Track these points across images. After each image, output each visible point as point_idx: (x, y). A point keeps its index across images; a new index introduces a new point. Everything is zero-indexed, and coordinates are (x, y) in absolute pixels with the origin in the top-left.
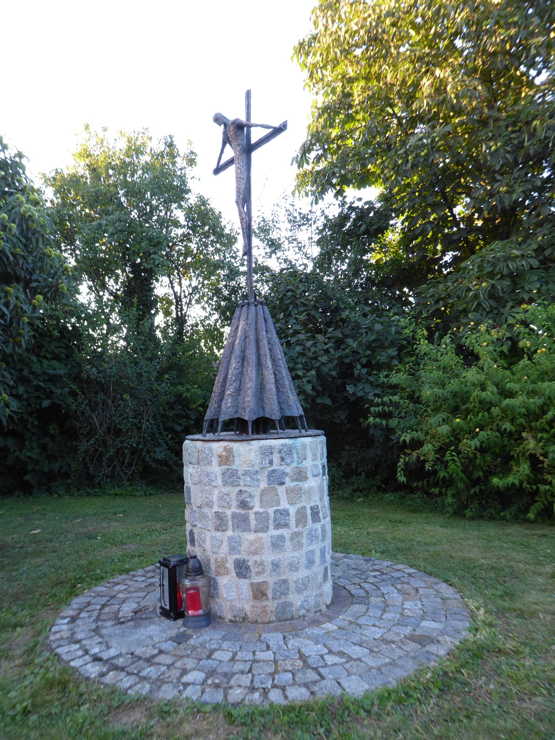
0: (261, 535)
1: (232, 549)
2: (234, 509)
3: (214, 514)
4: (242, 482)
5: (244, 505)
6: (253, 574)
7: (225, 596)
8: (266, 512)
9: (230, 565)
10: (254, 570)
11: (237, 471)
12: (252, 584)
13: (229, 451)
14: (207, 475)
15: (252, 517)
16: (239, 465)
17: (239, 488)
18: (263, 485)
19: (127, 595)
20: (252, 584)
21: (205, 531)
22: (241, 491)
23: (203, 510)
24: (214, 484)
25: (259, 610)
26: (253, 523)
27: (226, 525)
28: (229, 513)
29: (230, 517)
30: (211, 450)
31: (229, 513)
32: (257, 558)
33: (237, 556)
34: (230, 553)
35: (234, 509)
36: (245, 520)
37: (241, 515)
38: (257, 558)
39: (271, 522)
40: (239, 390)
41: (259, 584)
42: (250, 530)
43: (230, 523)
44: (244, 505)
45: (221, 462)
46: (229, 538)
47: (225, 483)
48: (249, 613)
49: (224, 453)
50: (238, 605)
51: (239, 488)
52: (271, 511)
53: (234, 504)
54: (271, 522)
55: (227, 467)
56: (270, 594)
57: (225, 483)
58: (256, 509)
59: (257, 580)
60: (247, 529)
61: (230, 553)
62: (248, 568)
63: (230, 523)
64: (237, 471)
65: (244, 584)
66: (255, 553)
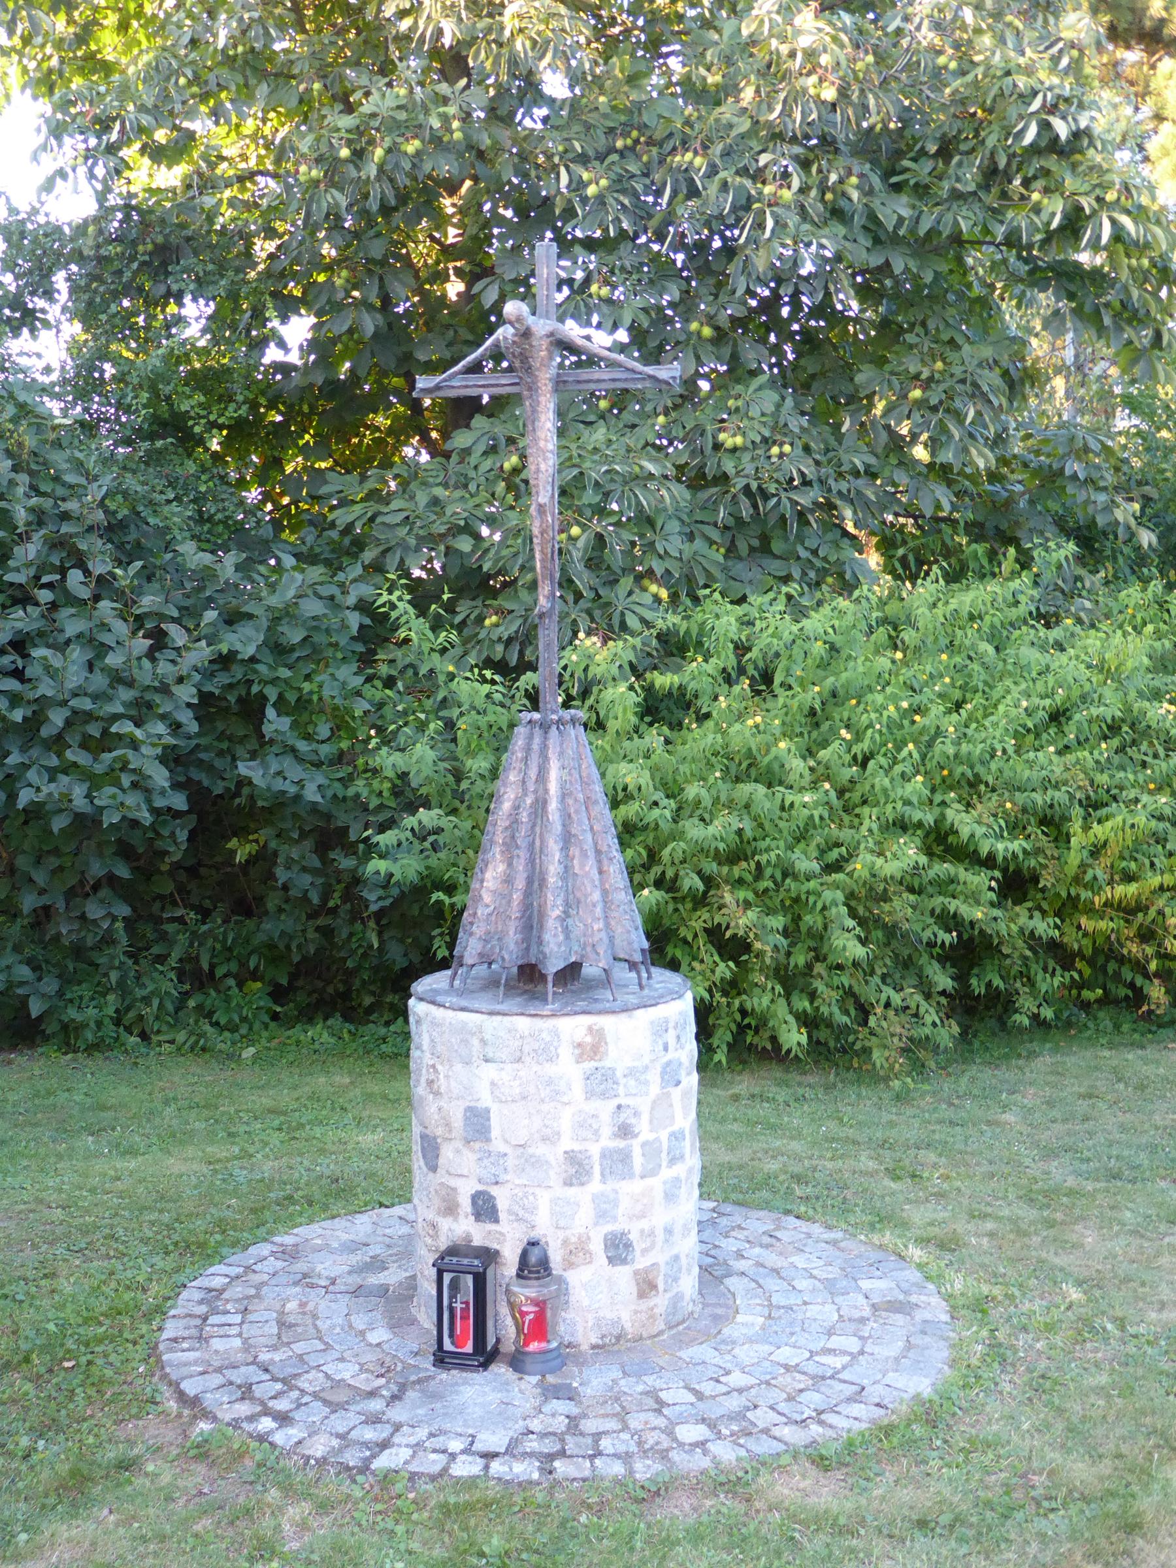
0: (649, 1181)
1: (602, 1215)
2: (608, 1141)
3: (561, 1157)
4: (621, 1090)
5: (625, 1131)
6: (638, 1253)
7: (586, 1302)
8: (657, 1139)
9: (597, 1246)
10: (638, 1246)
11: (613, 1070)
12: (636, 1273)
13: (599, 1036)
14: (550, 1082)
15: (637, 1152)
16: (617, 1058)
17: (616, 1102)
18: (655, 1089)
19: (985, 1289)
20: (636, 1273)
21: (538, 1191)
22: (619, 1107)
23: (530, 1151)
24: (565, 1099)
25: (644, 1316)
26: (638, 1160)
27: (588, 1173)
28: (595, 1150)
29: (596, 1158)
30: (556, 1034)
31: (595, 1150)
32: (644, 1224)
33: (610, 1228)
34: (596, 1224)
35: (608, 1141)
36: (625, 1157)
37: (619, 1151)
38: (644, 1224)
39: (664, 1155)
40: (571, 906)
41: (646, 1271)
42: (631, 1176)
43: (597, 1170)
44: (625, 1131)
45: (581, 1055)
46: (595, 1198)
47: (590, 1095)
48: (628, 1326)
49: (589, 1039)
50: (610, 1315)
51: (616, 1102)
52: (664, 1135)
53: (607, 1131)
54: (664, 1155)
55: (593, 1064)
56: (661, 1287)
57: (590, 1095)
58: (642, 1138)
59: (641, 1263)
60: (628, 1175)
61: (596, 1224)
62: (628, 1246)
63: (597, 1170)
64: (613, 1070)
65: (623, 1276)
66: (642, 1216)
